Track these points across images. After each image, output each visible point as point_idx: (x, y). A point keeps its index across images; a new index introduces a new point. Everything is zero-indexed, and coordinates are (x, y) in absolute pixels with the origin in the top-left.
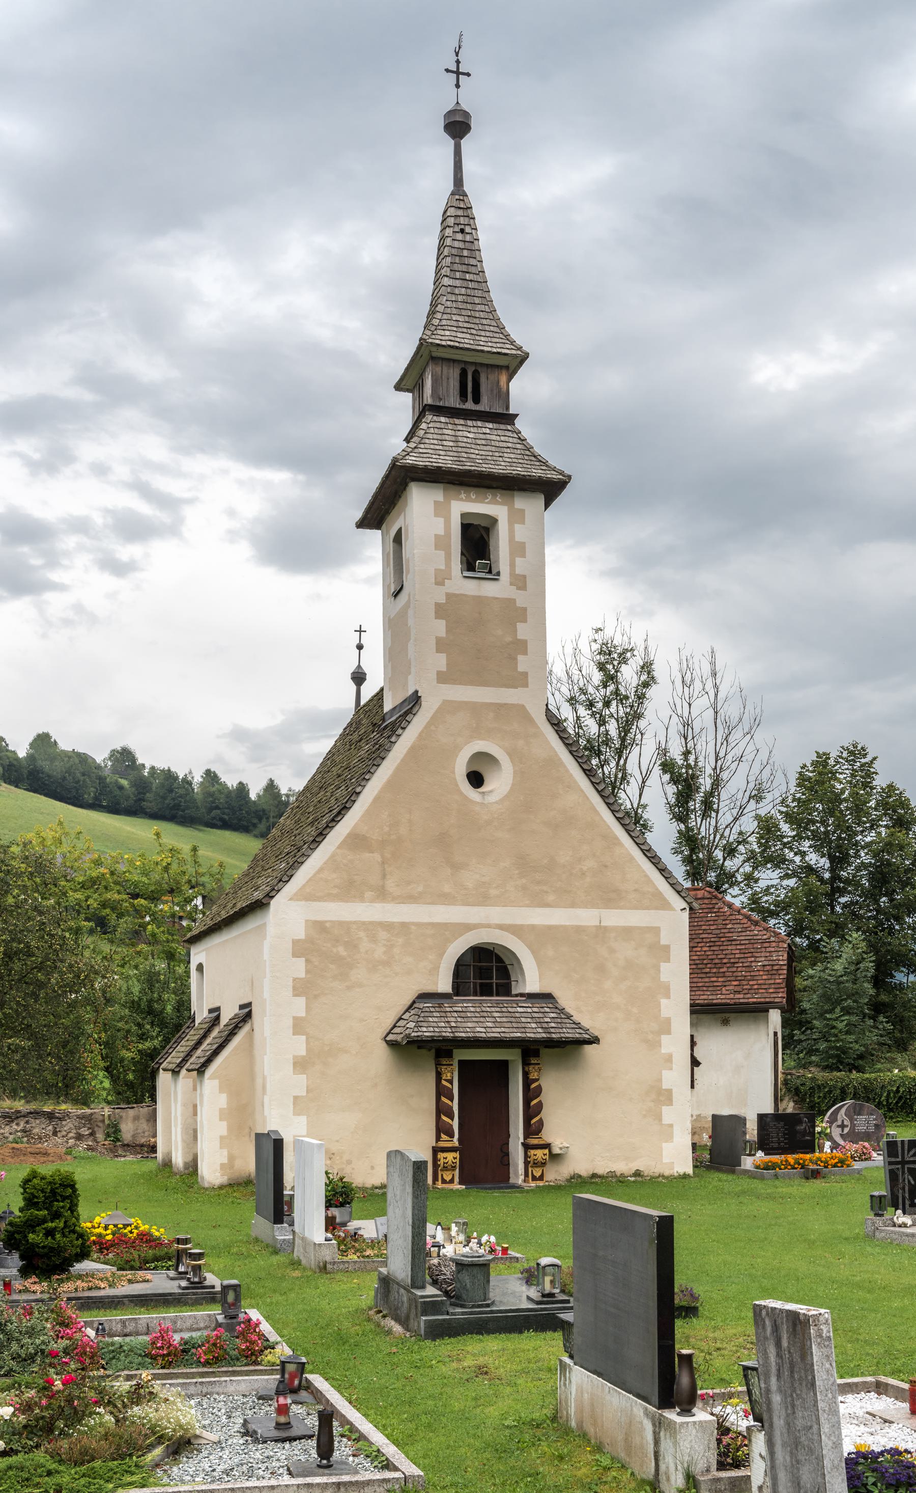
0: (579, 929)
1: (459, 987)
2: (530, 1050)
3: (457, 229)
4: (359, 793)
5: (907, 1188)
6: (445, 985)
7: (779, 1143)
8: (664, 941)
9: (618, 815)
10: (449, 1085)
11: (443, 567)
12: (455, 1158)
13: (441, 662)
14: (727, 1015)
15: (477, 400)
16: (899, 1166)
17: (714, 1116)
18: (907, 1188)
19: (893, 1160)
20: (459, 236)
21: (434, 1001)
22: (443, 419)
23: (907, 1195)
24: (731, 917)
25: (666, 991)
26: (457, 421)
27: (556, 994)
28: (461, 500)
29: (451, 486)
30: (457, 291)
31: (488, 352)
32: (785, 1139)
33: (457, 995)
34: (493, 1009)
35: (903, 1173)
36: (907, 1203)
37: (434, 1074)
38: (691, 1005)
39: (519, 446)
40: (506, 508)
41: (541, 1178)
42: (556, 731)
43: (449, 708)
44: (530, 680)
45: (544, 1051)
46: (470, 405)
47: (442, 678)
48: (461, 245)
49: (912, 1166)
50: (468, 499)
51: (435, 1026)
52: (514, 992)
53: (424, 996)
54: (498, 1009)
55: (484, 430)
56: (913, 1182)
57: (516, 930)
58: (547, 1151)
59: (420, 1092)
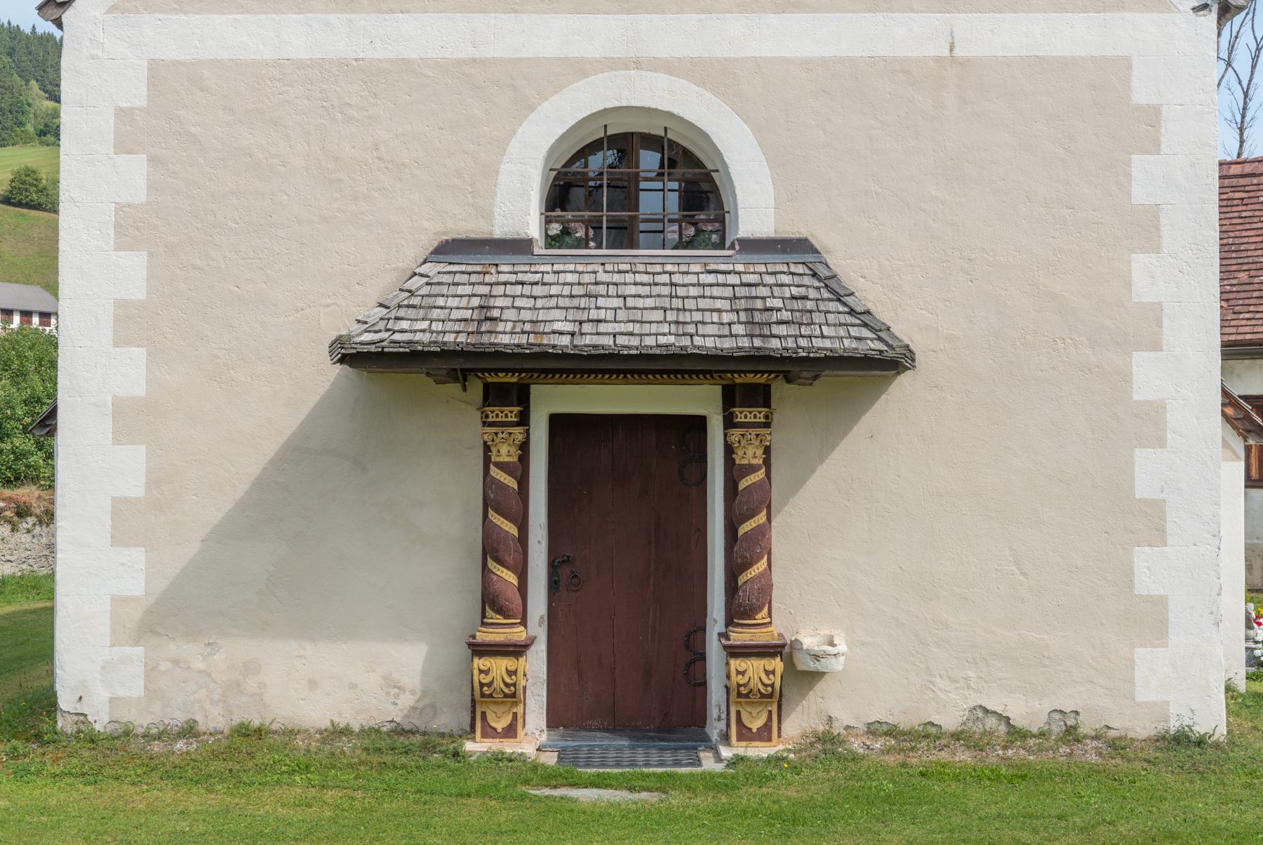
0: (902, 69)
2: (752, 381)
6: (521, 210)
8: (1141, 95)
27: (821, 238)
34: (629, 278)
41: (764, 734)
45: (780, 390)
57: (712, 74)
58: (777, 664)
59: (441, 477)
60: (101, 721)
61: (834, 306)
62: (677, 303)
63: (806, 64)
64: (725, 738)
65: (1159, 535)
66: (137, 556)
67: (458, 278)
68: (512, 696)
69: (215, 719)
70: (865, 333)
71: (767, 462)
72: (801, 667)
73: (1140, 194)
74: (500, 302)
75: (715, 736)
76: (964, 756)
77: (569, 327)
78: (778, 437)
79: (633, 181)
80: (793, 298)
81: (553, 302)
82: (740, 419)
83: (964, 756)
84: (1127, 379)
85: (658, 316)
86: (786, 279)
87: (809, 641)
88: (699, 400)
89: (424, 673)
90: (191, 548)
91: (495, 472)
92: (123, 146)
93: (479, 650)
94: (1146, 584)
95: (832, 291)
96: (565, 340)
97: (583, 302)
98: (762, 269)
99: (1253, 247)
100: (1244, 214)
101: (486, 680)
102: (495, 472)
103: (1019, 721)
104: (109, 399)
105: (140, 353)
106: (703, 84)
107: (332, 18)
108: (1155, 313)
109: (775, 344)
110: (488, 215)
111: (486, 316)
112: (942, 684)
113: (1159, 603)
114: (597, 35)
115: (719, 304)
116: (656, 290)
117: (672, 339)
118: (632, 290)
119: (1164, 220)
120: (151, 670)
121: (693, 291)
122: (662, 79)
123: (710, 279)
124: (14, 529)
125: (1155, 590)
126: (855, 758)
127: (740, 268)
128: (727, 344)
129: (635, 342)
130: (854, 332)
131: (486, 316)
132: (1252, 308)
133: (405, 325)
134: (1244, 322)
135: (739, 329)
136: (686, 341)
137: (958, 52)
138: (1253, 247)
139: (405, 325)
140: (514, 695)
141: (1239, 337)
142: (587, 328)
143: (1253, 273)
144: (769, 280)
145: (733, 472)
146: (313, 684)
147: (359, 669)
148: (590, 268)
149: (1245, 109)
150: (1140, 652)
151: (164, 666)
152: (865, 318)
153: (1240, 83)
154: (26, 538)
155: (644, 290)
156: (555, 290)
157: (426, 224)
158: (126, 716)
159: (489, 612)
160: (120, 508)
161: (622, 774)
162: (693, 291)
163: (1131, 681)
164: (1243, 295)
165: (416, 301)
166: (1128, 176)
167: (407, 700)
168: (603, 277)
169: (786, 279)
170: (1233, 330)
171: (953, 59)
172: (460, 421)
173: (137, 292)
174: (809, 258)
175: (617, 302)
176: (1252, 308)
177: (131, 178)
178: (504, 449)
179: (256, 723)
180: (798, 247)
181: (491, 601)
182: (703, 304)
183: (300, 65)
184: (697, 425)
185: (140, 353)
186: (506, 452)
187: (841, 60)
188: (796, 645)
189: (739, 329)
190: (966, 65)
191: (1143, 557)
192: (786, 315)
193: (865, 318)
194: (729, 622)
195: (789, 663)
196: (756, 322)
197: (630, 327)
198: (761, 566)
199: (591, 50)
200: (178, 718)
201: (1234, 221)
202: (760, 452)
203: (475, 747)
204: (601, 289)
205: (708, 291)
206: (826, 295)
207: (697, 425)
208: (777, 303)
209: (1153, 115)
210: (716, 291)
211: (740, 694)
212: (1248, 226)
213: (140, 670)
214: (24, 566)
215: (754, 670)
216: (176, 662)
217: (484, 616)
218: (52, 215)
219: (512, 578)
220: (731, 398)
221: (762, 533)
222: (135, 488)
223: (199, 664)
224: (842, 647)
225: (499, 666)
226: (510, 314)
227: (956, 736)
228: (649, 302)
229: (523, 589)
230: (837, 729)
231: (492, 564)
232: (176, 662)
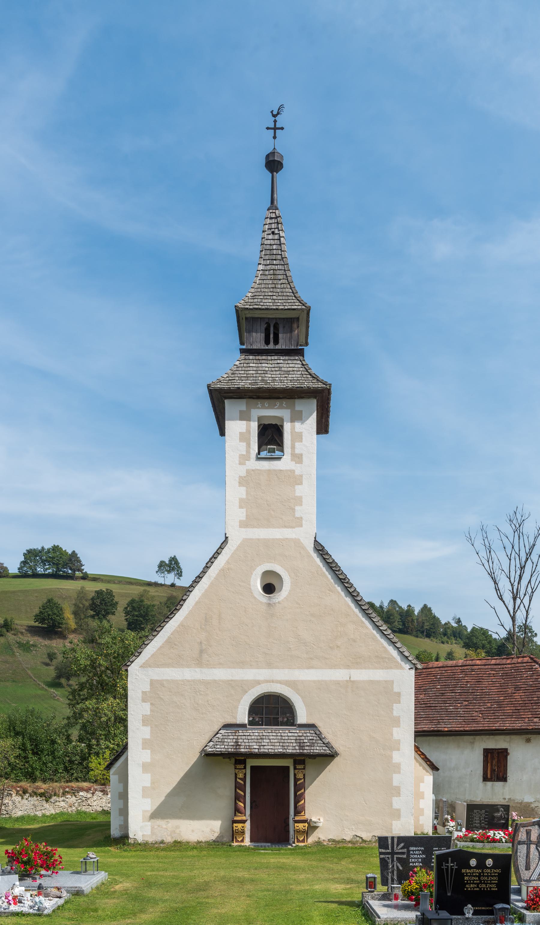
2: (300, 760)
3: (270, 232)
4: (185, 600)
5: (395, 873)
6: (243, 717)
7: (481, 824)
8: (396, 690)
9: (363, 608)
10: (242, 782)
11: (244, 453)
13: (242, 514)
14: (530, 736)
15: (276, 342)
16: (389, 856)
18: (395, 873)
19: (383, 851)
21: (232, 729)
23: (395, 877)
25: (396, 722)
27: (319, 724)
28: (259, 408)
31: (282, 309)
32: (486, 821)
34: (271, 734)
35: (393, 861)
38: (415, 732)
39: (301, 369)
40: (289, 410)
41: (303, 841)
43: (246, 543)
44: (304, 522)
46: (271, 346)
47: (244, 524)
49: (399, 856)
50: (263, 407)
55: (279, 361)
56: (401, 868)
57: (287, 683)
58: (306, 825)
60: (140, 840)
61: (320, 741)
62: (282, 741)
63: (314, 682)
64: (294, 843)
65: (398, 794)
66: (149, 800)
67: (229, 734)
68: (243, 832)
69: (169, 839)
70: (327, 749)
71: (304, 778)
72: (312, 825)
73: (395, 713)
74: (240, 741)
75: (291, 842)
76: (350, 845)
77: (257, 747)
78: (308, 771)
79: (272, 709)
80: (310, 739)
81: (253, 741)
82: (298, 768)
83: (350, 845)
84: (392, 758)
85: (278, 744)
86: (309, 734)
87: (314, 819)
88: (288, 763)
89: (220, 828)
90: (163, 798)
91: (238, 780)
92: (144, 701)
93: (234, 822)
94: (396, 806)
95: (319, 738)
96: (257, 750)
97: (260, 741)
98: (303, 732)
99: (494, 693)
100: (493, 680)
101: (237, 829)
102: (238, 780)
103: (364, 838)
104: (141, 762)
105: (149, 751)
106: (289, 686)
107: (196, 669)
108: (398, 742)
109: (305, 751)
110: (235, 718)
111: (237, 744)
112: (346, 830)
113: (399, 810)
114: (262, 674)
115: (293, 741)
116: (277, 737)
117: (281, 750)
118: (272, 737)
119: (401, 720)
120: (152, 828)
121: (286, 738)
122: (279, 685)
123: (290, 734)
124: (22, 798)
125: (398, 807)
126: (324, 845)
127: (298, 731)
128: (294, 751)
129: (273, 751)
130: (324, 748)
131: (237, 744)
132: (489, 717)
133: (218, 746)
134: (486, 723)
135: (297, 748)
136: (285, 751)
137: (352, 679)
138: (494, 693)
139: (218, 746)
140: (243, 832)
141: (483, 728)
142: (262, 747)
143: (492, 704)
144: (305, 735)
145: (296, 780)
146: (193, 831)
147: (204, 829)
148: (261, 731)
149: (526, 618)
150: (394, 822)
151: (156, 827)
152: (327, 745)
153: (525, 607)
154: (26, 802)
155: (275, 737)
156: (253, 737)
157: (220, 720)
159: (237, 813)
160: (144, 789)
162: (286, 738)
163: (392, 829)
164: (488, 712)
165: (220, 740)
166: (393, 709)
167: (216, 835)
168: (265, 734)
169: (309, 734)
170: (482, 725)
171: (350, 681)
172: (230, 768)
173: (148, 736)
174: (315, 729)
175: (268, 741)
176: (489, 717)
177: (146, 709)
178: (241, 775)
179: (179, 840)
180: (312, 726)
181: (237, 810)
182: (289, 741)
183: (188, 681)
184: (288, 768)
185: (149, 751)
186: (241, 775)
187: (323, 681)
188: (311, 820)
189: (297, 748)
190: (353, 682)
191: (395, 800)
192: (308, 744)
193: (327, 745)
194: (295, 815)
195: (309, 824)
196: (301, 747)
197: (272, 747)
198: (303, 802)
199: (261, 678)
200: (160, 839)
201: (490, 683)
202: (302, 775)
203: (235, 844)
204: (264, 737)
205: (290, 738)
206: (318, 739)
207: (288, 768)
208: (306, 741)
209: (399, 694)
210: (292, 738)
211: (298, 832)
212: (494, 685)
213: (150, 828)
214: (26, 812)
215: (301, 826)
216: (159, 826)
217: (235, 814)
219: (242, 805)
220: (296, 763)
221: (303, 794)
222: (148, 784)
223: (164, 826)
224: (322, 820)
225: (240, 826)
226: (243, 744)
227: (349, 842)
228: (276, 741)
229: (245, 807)
230: (321, 840)
231: (237, 802)
232: (159, 826)
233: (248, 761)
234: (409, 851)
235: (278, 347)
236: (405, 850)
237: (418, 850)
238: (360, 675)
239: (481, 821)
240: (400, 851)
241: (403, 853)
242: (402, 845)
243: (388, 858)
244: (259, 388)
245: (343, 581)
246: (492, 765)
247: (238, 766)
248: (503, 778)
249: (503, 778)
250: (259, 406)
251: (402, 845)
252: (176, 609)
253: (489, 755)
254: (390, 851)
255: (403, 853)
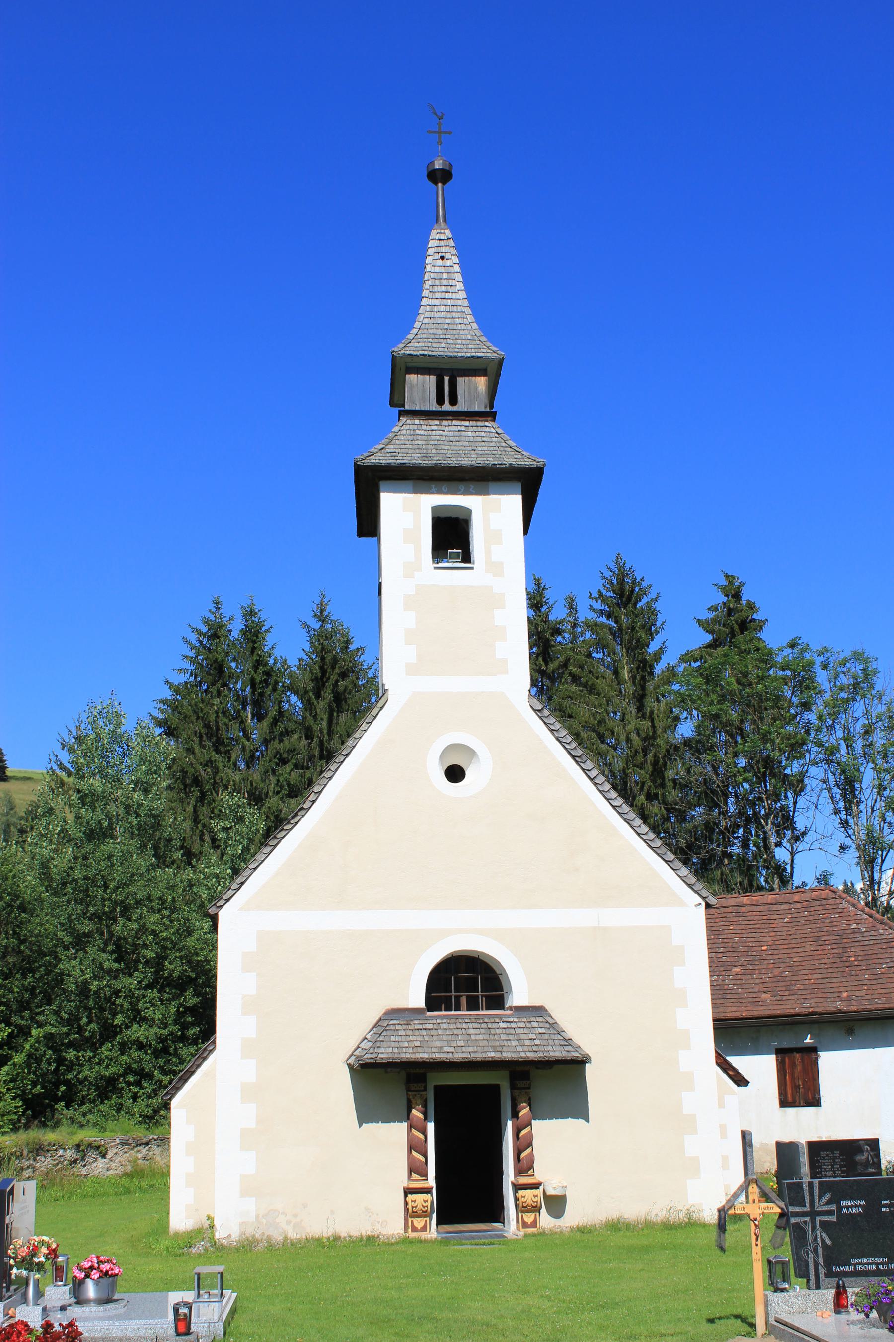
1: (432, 1003)
5: (820, 1250)
6: (417, 998)
12: (425, 1201)
15: (454, 401)
16: (807, 1219)
17: (779, 1145)
18: (820, 1250)
20: (440, 262)
22: (417, 422)
23: (821, 1260)
24: (855, 917)
26: (431, 422)
29: (421, 482)
30: (435, 309)
33: (429, 1010)
34: (470, 1025)
35: (814, 1228)
36: (822, 1271)
37: (405, 1102)
42: (540, 717)
46: (447, 406)
48: (442, 270)
50: (439, 492)
51: (408, 1046)
52: (507, 1006)
53: (394, 1013)
54: (475, 1025)
56: (829, 1242)
79: (465, 981)
82: (519, 1086)
98: (525, 1020)
127: (515, 1020)
158: (250, 1231)
161: (472, 1249)
180: (538, 1010)
184: (496, 1088)
207: (496, 1088)
218: (722, 1016)
233: (430, 1075)
234: (840, 1208)
235: (456, 408)
236: (833, 1207)
237: (856, 1206)
238: (614, 917)
239: (834, 1173)
240: (826, 1208)
241: (830, 1213)
242: (828, 1196)
243: (805, 1222)
244: (436, 465)
245: (577, 759)
246: (793, 1078)
247: (414, 1086)
248: (814, 1101)
249: (814, 1101)
250: (434, 489)
251: (828, 1196)
252: (302, 808)
253: (787, 1060)
254: (807, 1209)
255: (830, 1213)
